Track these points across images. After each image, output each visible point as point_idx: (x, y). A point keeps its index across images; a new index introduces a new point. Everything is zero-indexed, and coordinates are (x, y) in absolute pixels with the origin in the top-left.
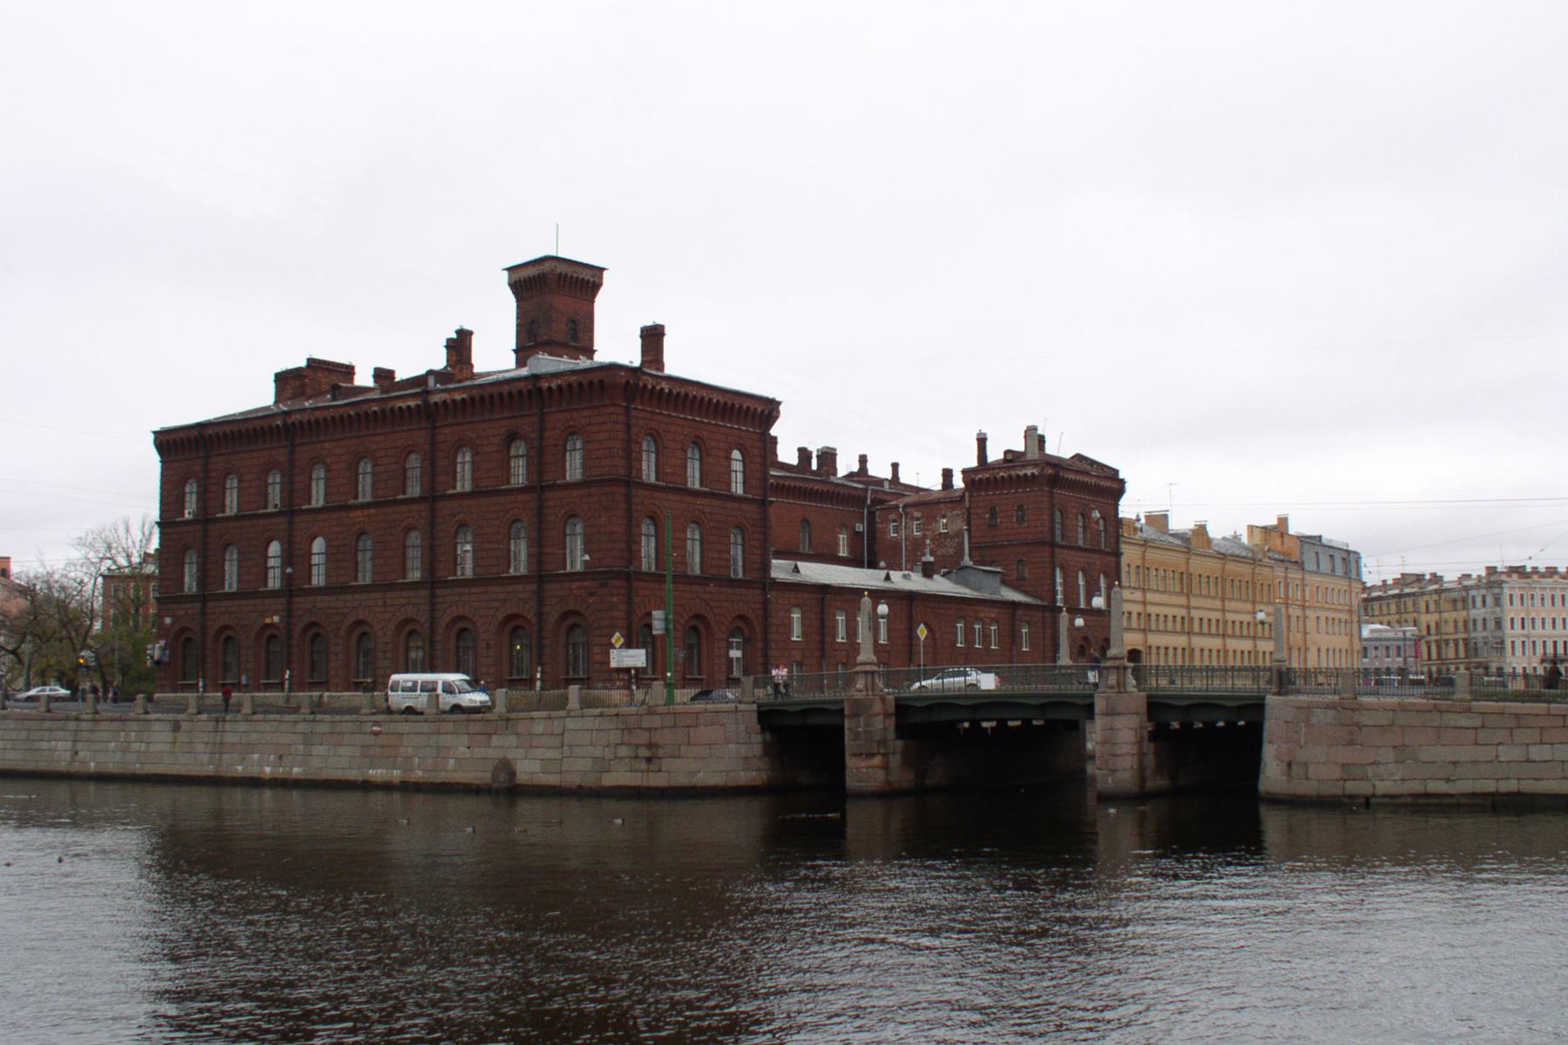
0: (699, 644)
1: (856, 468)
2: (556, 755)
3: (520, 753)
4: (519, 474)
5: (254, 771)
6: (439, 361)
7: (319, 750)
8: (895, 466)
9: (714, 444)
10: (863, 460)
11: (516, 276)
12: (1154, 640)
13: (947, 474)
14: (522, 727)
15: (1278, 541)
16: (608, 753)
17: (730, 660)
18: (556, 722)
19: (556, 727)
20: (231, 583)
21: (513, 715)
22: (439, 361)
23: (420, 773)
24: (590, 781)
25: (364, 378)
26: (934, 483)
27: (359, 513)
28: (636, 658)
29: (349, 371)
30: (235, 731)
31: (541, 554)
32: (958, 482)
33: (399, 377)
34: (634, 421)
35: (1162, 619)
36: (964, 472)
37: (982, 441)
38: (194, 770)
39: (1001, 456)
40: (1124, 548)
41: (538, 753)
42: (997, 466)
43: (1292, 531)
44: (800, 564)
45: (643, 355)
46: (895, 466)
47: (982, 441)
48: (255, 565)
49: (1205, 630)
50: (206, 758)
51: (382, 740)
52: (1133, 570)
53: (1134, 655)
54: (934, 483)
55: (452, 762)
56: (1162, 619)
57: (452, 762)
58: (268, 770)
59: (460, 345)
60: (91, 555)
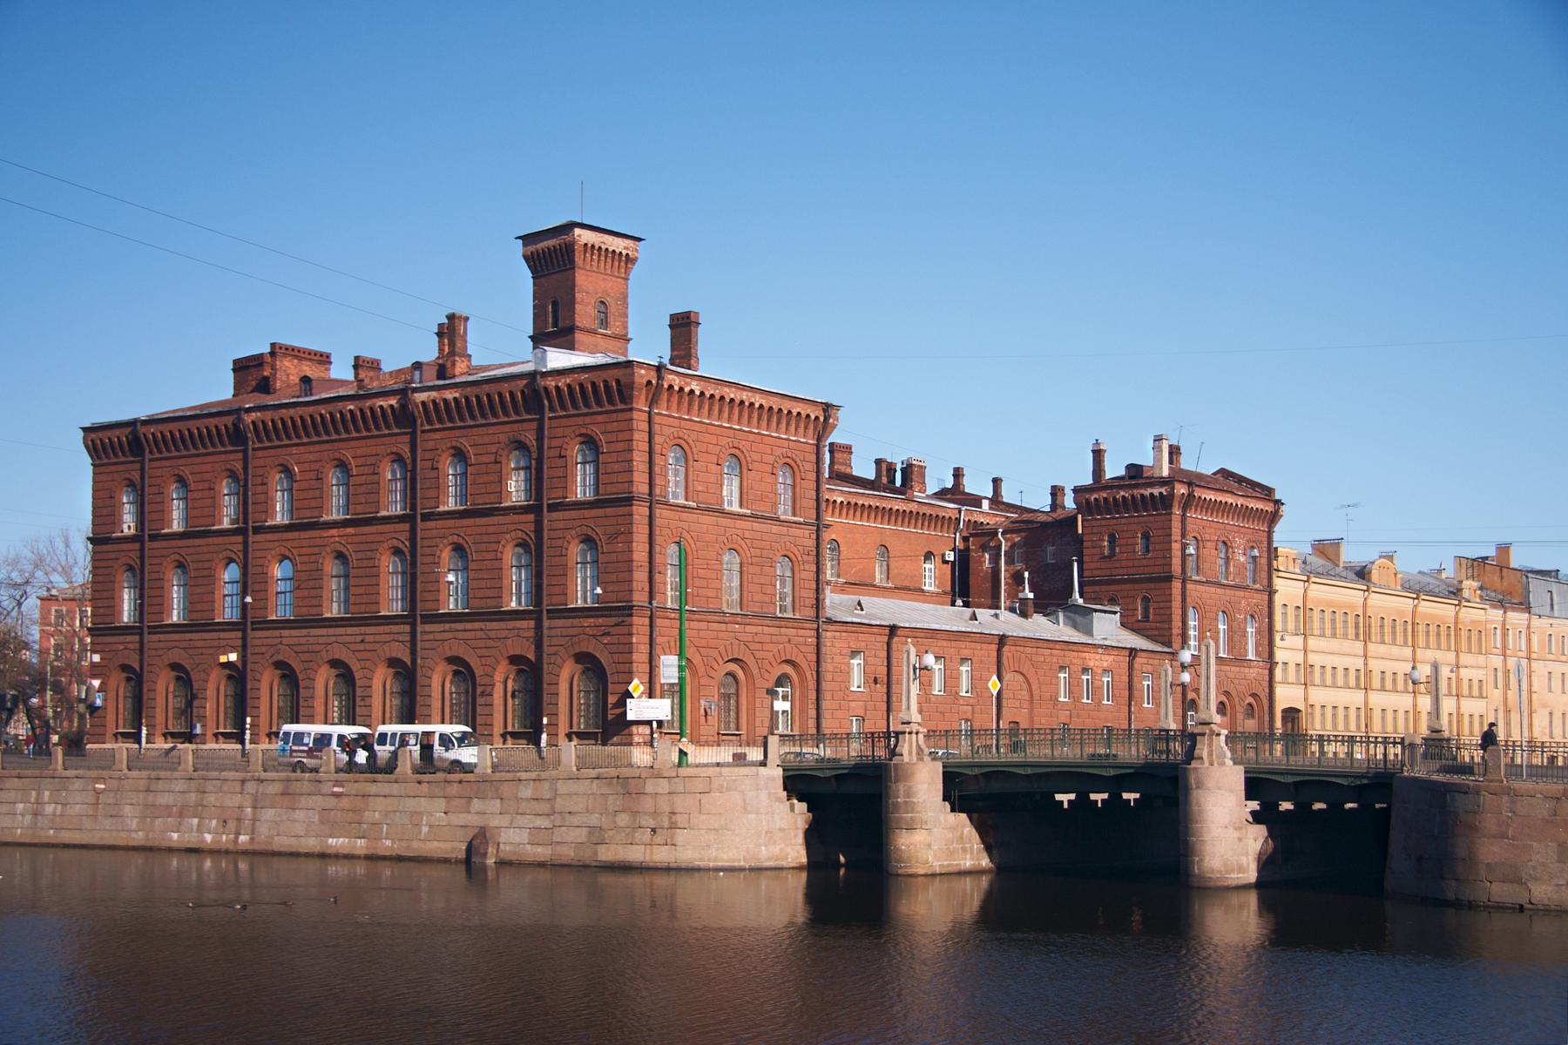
0: (737, 694)
1: (949, 484)
2: (544, 823)
3: (503, 821)
4: (515, 488)
5: (191, 839)
6: (429, 351)
7: (268, 814)
8: (996, 482)
9: (756, 457)
10: (958, 474)
11: (532, 248)
12: (1318, 696)
13: (1056, 492)
14: (506, 789)
15: (1496, 578)
16: (605, 821)
17: (774, 715)
18: (546, 785)
19: (545, 790)
20: (127, 615)
21: (498, 776)
22: (429, 351)
23: (388, 843)
24: (586, 855)
25: (341, 370)
26: (1042, 502)
27: (334, 532)
28: (661, 709)
29: (324, 359)
30: (172, 792)
31: (141, 605)
32: (1069, 502)
33: (387, 367)
34: (657, 428)
35: (1329, 671)
36: (1076, 490)
37: (1098, 455)
38: (120, 839)
39: (1122, 472)
40: (1278, 584)
41: (526, 821)
42: (1117, 483)
43: (1515, 563)
44: (865, 600)
45: (673, 349)
46: (996, 482)
47: (1098, 455)
48: (483, 578)
49: (1340, 682)
50: (134, 824)
51: (345, 802)
52: (1291, 611)
53: (1291, 714)
54: (1042, 502)
55: (425, 829)
56: (1329, 671)
57: (425, 829)
58: (208, 838)
59: (451, 331)
60: (14, 575)
